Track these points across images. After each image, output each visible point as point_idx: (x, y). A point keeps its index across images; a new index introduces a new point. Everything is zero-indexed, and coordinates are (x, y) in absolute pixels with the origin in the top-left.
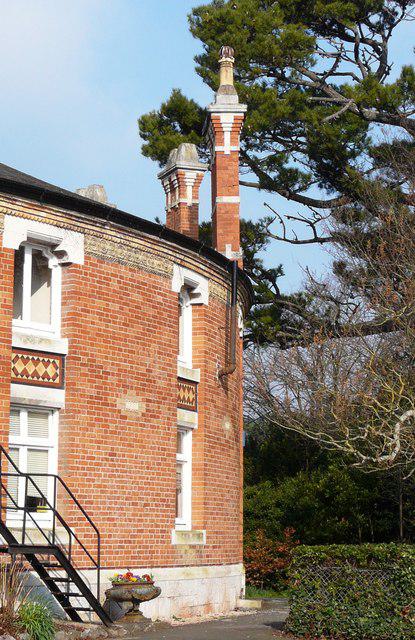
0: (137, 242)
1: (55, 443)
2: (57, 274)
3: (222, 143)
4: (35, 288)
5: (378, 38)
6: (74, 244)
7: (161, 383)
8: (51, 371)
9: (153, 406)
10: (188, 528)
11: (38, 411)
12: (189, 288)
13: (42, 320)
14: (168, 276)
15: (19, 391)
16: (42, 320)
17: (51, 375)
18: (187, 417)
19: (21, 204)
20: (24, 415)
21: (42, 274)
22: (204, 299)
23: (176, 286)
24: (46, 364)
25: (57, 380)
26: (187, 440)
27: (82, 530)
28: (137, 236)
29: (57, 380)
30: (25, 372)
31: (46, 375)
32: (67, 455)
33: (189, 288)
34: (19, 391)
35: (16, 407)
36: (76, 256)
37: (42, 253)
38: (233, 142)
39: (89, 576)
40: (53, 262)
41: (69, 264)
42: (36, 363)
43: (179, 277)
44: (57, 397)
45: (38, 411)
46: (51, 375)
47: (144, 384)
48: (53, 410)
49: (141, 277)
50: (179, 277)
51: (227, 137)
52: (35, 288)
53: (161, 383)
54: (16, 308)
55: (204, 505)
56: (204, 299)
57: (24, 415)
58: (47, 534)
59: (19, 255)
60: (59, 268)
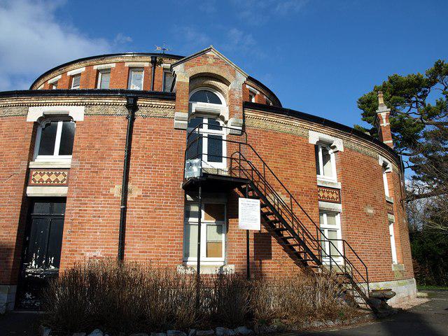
0: (364, 144)
1: (340, 228)
2: (333, 156)
3: (383, 123)
4: (324, 163)
5: (422, 100)
6: (339, 144)
7: (380, 202)
8: (335, 196)
9: (378, 211)
10: (396, 263)
11: (332, 213)
12: (385, 166)
13: (329, 174)
14: (377, 159)
15: (323, 205)
16: (329, 174)
17: (335, 198)
18: (390, 217)
19: (314, 126)
20: (325, 215)
21: (326, 158)
22: (391, 170)
23: (381, 163)
24: (333, 193)
25: (66, 173)
26: (391, 227)
27: (359, 266)
28: (364, 141)
29: (65, 182)
30: (324, 196)
31: (333, 198)
32: (346, 231)
33: (385, 166)
34: (323, 205)
35: (322, 212)
36: (340, 148)
37: (325, 146)
38: (387, 122)
39: (364, 287)
40: (331, 151)
41: (338, 151)
42: (328, 192)
43: (381, 160)
44: (339, 207)
45: (332, 213)
46: (335, 198)
47: (374, 203)
48: (337, 213)
49: (366, 158)
50: (381, 160)
51: (384, 120)
52: (324, 163)
53: (380, 202)
54: (318, 173)
55: (401, 253)
56: (391, 170)
57: (325, 215)
58: (341, 267)
59: (316, 147)
60: (334, 154)
